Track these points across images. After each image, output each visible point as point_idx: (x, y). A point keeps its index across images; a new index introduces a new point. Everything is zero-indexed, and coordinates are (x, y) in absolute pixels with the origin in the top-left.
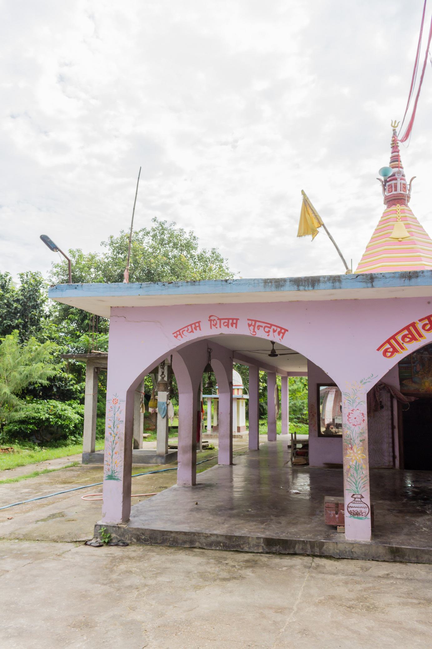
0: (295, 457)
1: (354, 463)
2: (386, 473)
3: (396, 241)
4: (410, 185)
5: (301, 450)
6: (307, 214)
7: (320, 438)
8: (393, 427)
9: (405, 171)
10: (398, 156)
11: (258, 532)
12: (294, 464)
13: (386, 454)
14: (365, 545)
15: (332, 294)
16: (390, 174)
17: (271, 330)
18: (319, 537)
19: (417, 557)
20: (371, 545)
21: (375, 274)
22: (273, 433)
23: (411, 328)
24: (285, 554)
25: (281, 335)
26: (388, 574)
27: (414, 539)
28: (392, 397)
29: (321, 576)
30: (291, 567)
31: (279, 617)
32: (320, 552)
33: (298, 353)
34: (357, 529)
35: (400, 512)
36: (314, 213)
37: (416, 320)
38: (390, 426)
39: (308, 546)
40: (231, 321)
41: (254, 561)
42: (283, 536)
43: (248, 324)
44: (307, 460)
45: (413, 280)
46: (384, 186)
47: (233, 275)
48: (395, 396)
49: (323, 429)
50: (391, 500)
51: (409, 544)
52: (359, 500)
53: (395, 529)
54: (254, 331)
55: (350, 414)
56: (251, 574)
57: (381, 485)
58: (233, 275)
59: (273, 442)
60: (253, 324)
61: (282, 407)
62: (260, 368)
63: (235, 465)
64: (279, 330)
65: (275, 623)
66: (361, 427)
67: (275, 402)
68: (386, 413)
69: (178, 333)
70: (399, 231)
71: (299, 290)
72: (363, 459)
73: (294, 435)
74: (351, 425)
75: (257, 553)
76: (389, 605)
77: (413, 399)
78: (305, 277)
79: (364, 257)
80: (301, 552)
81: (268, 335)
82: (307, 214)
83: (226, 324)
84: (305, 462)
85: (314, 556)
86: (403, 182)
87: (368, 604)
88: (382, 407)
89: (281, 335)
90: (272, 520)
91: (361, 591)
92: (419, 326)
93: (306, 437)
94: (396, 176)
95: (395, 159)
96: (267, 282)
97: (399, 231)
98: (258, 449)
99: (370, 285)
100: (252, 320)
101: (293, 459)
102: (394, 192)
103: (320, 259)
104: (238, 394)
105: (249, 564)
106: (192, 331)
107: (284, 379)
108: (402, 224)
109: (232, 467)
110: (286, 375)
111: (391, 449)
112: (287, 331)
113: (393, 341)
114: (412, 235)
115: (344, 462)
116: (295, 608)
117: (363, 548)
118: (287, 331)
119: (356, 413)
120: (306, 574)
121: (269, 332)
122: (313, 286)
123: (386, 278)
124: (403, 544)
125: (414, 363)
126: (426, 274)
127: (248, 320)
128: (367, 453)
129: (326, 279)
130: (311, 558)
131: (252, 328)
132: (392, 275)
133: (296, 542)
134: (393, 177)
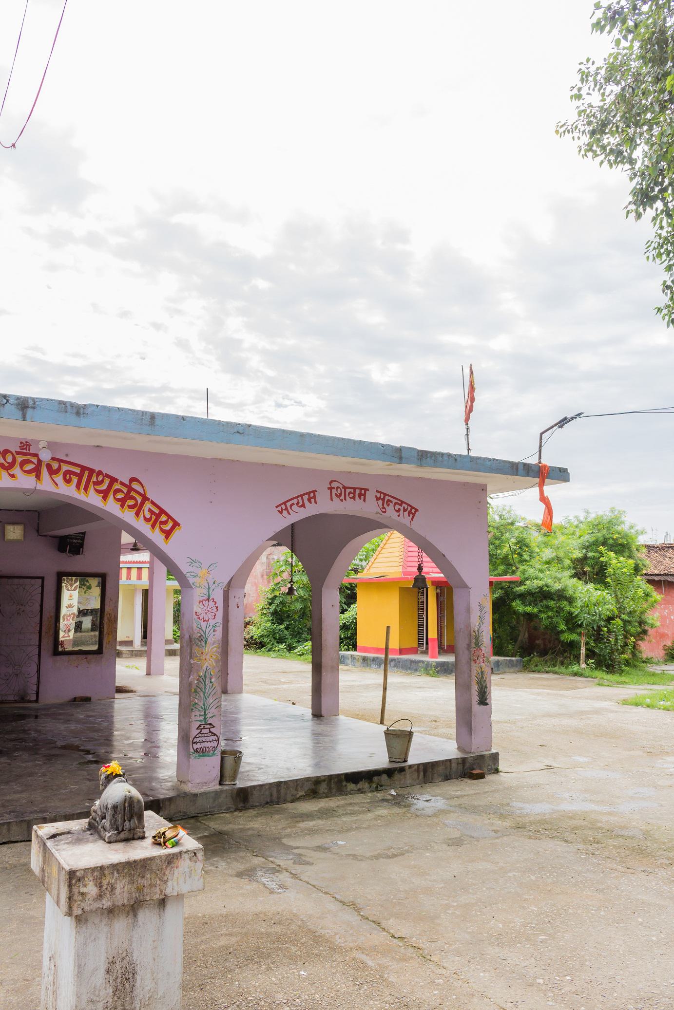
40: (357, 491)
69: (283, 508)
83: (352, 495)
100: (381, 493)
106: (303, 506)
121: (398, 511)
131: (380, 502)
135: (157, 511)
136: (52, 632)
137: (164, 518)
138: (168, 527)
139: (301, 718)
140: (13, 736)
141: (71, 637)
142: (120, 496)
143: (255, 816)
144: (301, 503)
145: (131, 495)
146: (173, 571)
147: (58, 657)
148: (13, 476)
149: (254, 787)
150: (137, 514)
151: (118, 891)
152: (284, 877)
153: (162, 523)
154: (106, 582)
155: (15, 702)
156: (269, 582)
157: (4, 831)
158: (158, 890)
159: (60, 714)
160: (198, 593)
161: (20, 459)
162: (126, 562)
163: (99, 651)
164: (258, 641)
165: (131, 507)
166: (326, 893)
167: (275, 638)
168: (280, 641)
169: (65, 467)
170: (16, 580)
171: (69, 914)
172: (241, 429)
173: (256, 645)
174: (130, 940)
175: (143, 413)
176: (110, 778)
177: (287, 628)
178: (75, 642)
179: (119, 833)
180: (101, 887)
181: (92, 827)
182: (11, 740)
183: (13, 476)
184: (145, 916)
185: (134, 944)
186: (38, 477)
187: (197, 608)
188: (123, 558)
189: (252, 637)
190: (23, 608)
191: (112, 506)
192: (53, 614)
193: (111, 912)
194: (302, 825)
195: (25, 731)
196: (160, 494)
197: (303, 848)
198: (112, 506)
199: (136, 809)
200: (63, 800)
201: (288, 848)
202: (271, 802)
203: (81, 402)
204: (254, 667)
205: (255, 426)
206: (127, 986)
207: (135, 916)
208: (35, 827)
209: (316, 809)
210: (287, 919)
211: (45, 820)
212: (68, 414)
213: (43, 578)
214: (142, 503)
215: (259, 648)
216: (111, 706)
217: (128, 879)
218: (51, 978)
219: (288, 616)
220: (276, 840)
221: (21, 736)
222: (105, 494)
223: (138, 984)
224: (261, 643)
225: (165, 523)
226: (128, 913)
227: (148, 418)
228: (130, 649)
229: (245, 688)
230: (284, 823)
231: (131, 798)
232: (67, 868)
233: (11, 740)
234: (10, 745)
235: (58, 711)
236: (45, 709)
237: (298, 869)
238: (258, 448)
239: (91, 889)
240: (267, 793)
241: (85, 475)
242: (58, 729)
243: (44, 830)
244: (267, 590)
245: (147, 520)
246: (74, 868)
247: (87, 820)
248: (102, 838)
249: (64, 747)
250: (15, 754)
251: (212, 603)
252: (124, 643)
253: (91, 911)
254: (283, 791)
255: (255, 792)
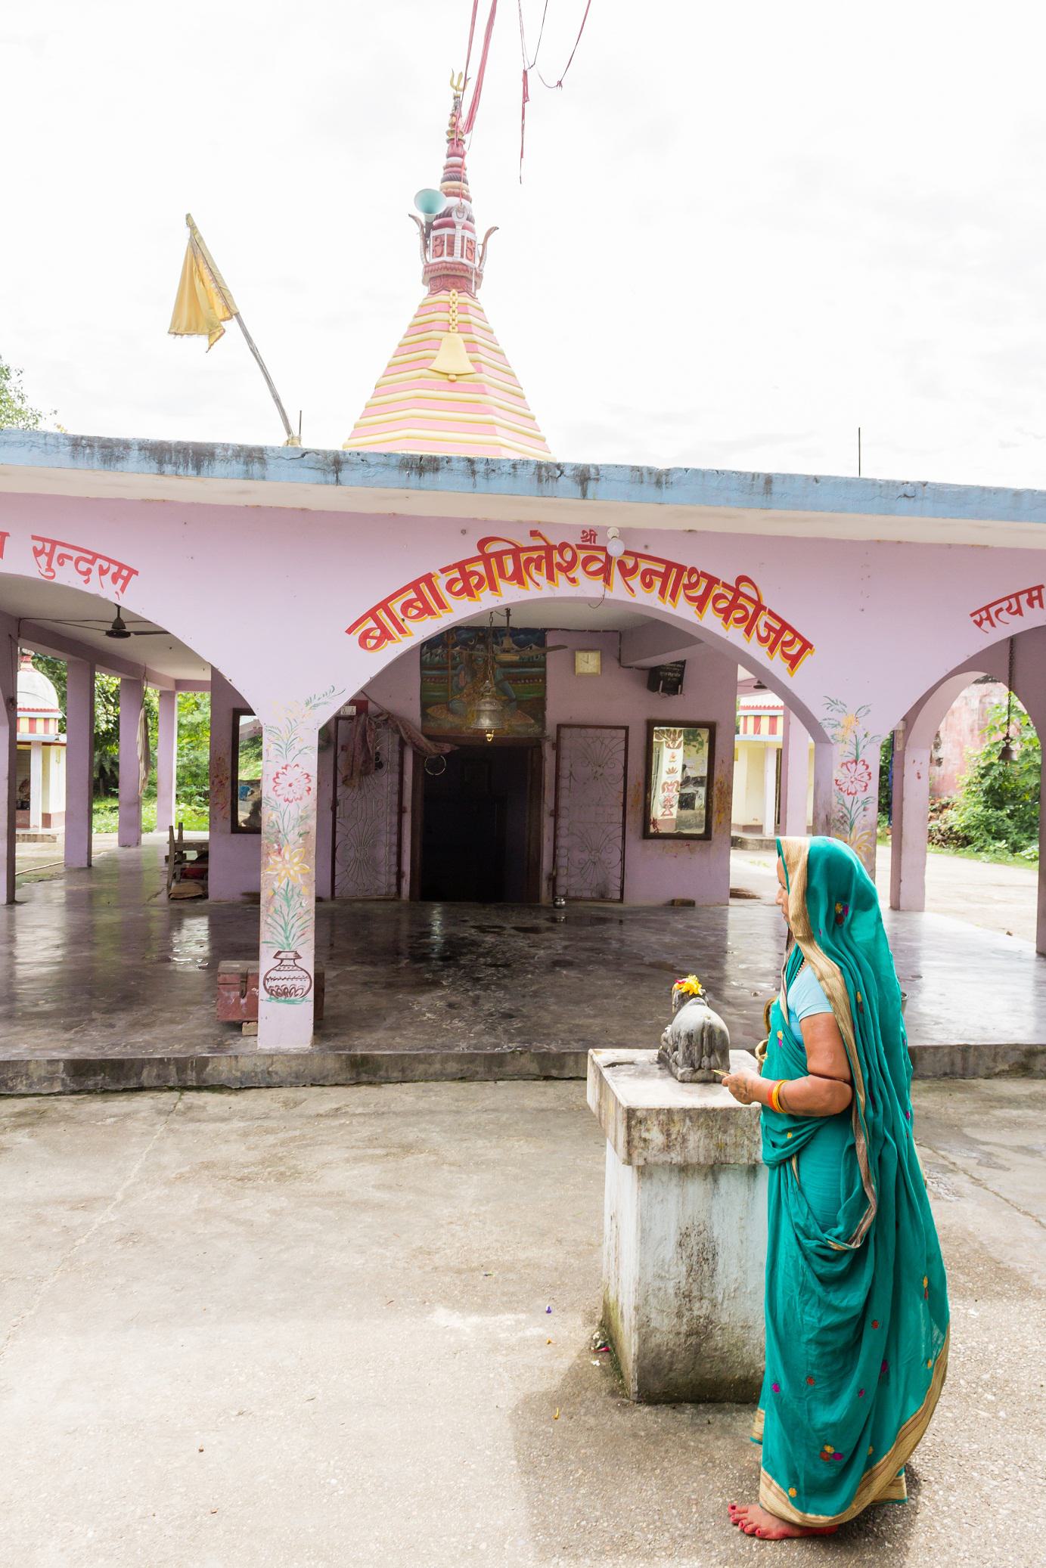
0: (178, 882)
1: (283, 885)
2: (378, 909)
3: (444, 380)
4: (484, 245)
5: (194, 866)
6: (197, 281)
7: (234, 836)
8: (401, 811)
9: (475, 208)
10: (461, 166)
11: (53, 1049)
12: (173, 898)
13: (383, 869)
14: (297, 1056)
15: (243, 492)
16: (440, 211)
17: (95, 569)
18: (198, 1049)
19: (403, 1070)
20: (311, 1054)
21: (344, 454)
22: (131, 829)
23: (423, 586)
24: (116, 1091)
25: (120, 582)
26: (337, 1109)
27: (402, 1036)
28: (402, 744)
29: (192, 1126)
30: (127, 1115)
31: (78, 1218)
32: (198, 1079)
33: (166, 632)
34: (285, 1025)
35: (389, 985)
36: (215, 280)
37: (435, 570)
38: (395, 809)
39: (172, 1069)
41: (37, 1112)
42: (114, 1053)
43: (35, 548)
44: (205, 887)
45: (428, 477)
46: (426, 236)
47: (37, 417)
48: (408, 741)
49: (243, 815)
50: (373, 964)
51: (390, 1047)
52: (291, 963)
53: (368, 1020)
54: (49, 569)
55: (287, 779)
56: (26, 1140)
57: (341, 925)
58: (37, 417)
59: (133, 850)
60: (47, 550)
61: (161, 763)
62: (97, 666)
63: (21, 903)
64: (114, 569)
65: (66, 1230)
66: (302, 804)
67: (140, 752)
68: (386, 779)
69: (984, 616)
70: (452, 357)
71: (162, 473)
72: (303, 875)
73: (176, 832)
74: (281, 800)
75: (49, 1095)
76: (324, 1165)
77: (447, 748)
78: (179, 443)
79: (370, 410)
80: (155, 1084)
81: (87, 581)
82: (197, 281)
84: (200, 892)
85: (185, 1088)
86: (468, 234)
87: (282, 1169)
88: (380, 765)
89: (120, 582)
90: (93, 1020)
91: (274, 1146)
92: (441, 582)
93: (204, 836)
94: (454, 218)
95: (455, 174)
96: (78, 445)
97: (452, 357)
98: (90, 865)
99: (332, 478)
100: (44, 540)
101: (173, 885)
102: (446, 258)
103: (209, 400)
104: (46, 731)
105: (22, 1120)
106: (1019, 611)
107: (167, 697)
108: (459, 338)
109: (12, 909)
110: (171, 688)
111: (394, 859)
112: (136, 573)
113: (382, 614)
114: (480, 371)
115: (263, 886)
116: (119, 1196)
117: (293, 1064)
118: (136, 573)
119: (294, 774)
120: (158, 1127)
121: (88, 572)
122: (198, 467)
123: (369, 466)
124: (378, 1047)
125: (454, 668)
126: (455, 465)
127: (34, 538)
128: (313, 862)
129: (230, 452)
130: (177, 1094)
132: (383, 459)
133: (143, 1063)
134: (446, 220)
135: (777, 626)
136: (641, 805)
137: (787, 636)
138: (793, 651)
139: (1018, 956)
140: (589, 944)
141: (674, 816)
142: (722, 604)
143: (925, 1091)
144: (1015, 608)
145: (739, 602)
146: (794, 704)
147: (649, 842)
148: (573, 580)
149: (925, 1048)
150: (748, 631)
151: (691, 1144)
152: (960, 1181)
153: (785, 644)
154: (712, 734)
155: (593, 900)
156: (982, 741)
157: (571, 1063)
158: (745, 1153)
159: (648, 921)
160: (841, 752)
161: (582, 555)
162: (748, 708)
163: (707, 836)
164: (962, 834)
165: (738, 621)
166: (1026, 1213)
167: (989, 831)
168: (998, 836)
169: (644, 565)
170: (590, 731)
171: (629, 1161)
172: (909, 491)
173: (960, 840)
174: (709, 1210)
175: (755, 476)
176: (685, 998)
177: (1010, 816)
178: (680, 822)
179: (695, 1071)
180: (669, 1135)
181: (662, 1060)
182: (586, 950)
183: (573, 580)
184: (728, 1182)
185: (714, 1218)
186: (607, 581)
187: (838, 773)
188: (744, 700)
189: (950, 829)
190: (600, 770)
191: (710, 621)
192: (641, 780)
193: (684, 1170)
194: (999, 1113)
195: (604, 940)
196: (781, 599)
197: (995, 1144)
198: (710, 621)
199: (718, 1041)
200: (646, 1033)
201: (972, 1143)
202: (952, 1073)
203: (661, 466)
204: (945, 872)
205: (933, 484)
206: (705, 1267)
207: (715, 1181)
208: (591, 1051)
209: (1027, 1093)
210: (957, 1237)
211: (604, 1046)
212: (645, 485)
213: (626, 728)
214: (756, 615)
215: (962, 846)
216: (723, 915)
217: (705, 1131)
218: (613, 1242)
219: (1014, 797)
220: (954, 1129)
221: (598, 945)
222: (700, 603)
223: (720, 1268)
224: (966, 837)
225: (790, 643)
226: (706, 1175)
227: (761, 482)
228: (759, 837)
229: (927, 904)
230: (969, 1106)
231: (711, 1026)
232: (625, 1105)
233: (586, 950)
234: (584, 955)
235: (646, 916)
236: (631, 913)
237: (984, 1173)
238: (940, 521)
239: (656, 1136)
240: (946, 1059)
241: (672, 576)
242: (646, 940)
243: (601, 1056)
244: (978, 753)
245: (763, 640)
246: (633, 1105)
247: (657, 1051)
248: (673, 1075)
249: (652, 965)
250: (590, 968)
251: (861, 768)
252: (747, 828)
253: (656, 1165)
254: (971, 1060)
255: (926, 1056)
